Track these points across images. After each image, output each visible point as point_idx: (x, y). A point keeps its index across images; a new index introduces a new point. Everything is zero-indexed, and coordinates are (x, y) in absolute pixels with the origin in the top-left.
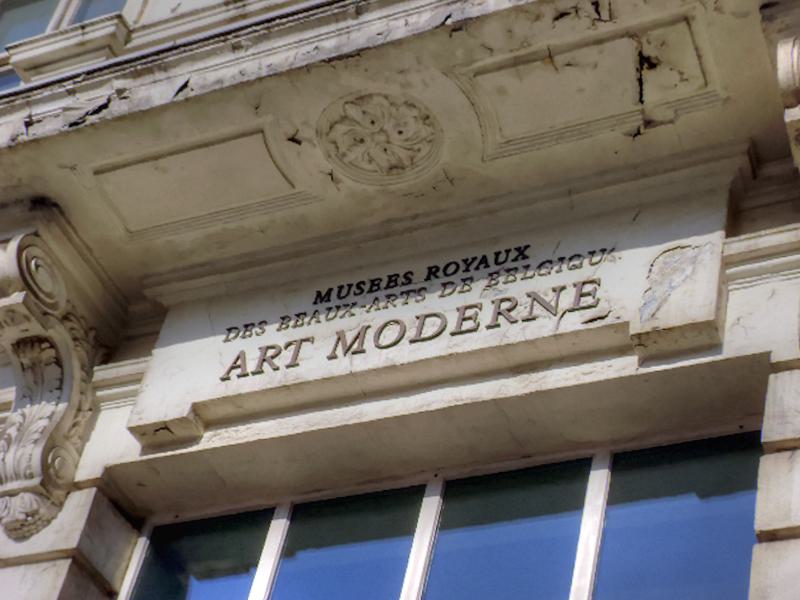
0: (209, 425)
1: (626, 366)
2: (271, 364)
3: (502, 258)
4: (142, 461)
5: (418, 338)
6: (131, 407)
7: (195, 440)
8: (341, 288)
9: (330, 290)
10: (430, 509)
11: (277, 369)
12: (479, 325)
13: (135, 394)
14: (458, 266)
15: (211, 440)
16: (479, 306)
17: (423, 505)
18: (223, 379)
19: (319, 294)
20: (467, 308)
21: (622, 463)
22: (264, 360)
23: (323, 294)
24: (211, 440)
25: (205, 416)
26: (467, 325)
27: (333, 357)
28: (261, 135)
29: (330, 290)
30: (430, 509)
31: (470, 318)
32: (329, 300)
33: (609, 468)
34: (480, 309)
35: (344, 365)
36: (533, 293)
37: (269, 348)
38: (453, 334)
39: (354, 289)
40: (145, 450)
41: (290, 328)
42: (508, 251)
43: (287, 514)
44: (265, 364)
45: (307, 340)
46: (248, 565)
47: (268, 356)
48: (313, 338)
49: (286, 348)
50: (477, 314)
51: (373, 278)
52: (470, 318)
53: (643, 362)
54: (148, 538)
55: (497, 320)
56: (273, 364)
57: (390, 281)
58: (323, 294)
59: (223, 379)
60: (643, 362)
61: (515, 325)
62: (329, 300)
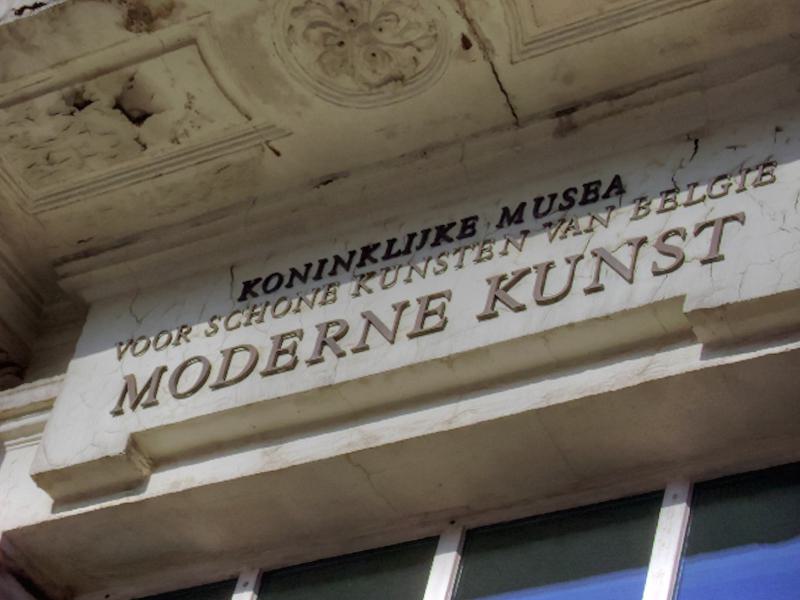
0: (159, 463)
1: (687, 359)
2: (335, 349)
3: (544, 207)
4: (54, 521)
5: (222, 382)
6: (36, 446)
7: (138, 484)
8: (539, 201)
9: (523, 205)
10: (672, 524)
11: (341, 355)
12: (445, 322)
13: (40, 427)
14: (281, 279)
15: (161, 483)
16: (300, 334)
17: (434, 563)
18: (482, 318)
19: (506, 210)
20: (432, 298)
21: (704, 494)
22: (324, 343)
23: (512, 212)
24: (161, 483)
25: (147, 454)
26: (284, 360)
27: (118, 412)
28: (194, 47)
29: (523, 205)
30: (672, 524)
31: (435, 313)
32: (520, 221)
33: (458, 551)
34: (449, 300)
35: (509, 326)
36: (602, 249)
37: (328, 325)
38: (411, 336)
39: (560, 200)
40: (60, 503)
41: (653, 214)
42: (553, 197)
43: (686, 495)
44: (327, 349)
45: (734, 218)
46: (640, 559)
47: (331, 338)
48: (450, 294)
49: (698, 232)
50: (443, 306)
51: (586, 182)
52: (435, 313)
53: (705, 355)
54: (255, 592)
55: (320, 353)
56: (338, 348)
57: (464, 229)
58: (512, 212)
59: (482, 318)
60: (711, 349)
61: (521, 313)
62: (520, 221)
